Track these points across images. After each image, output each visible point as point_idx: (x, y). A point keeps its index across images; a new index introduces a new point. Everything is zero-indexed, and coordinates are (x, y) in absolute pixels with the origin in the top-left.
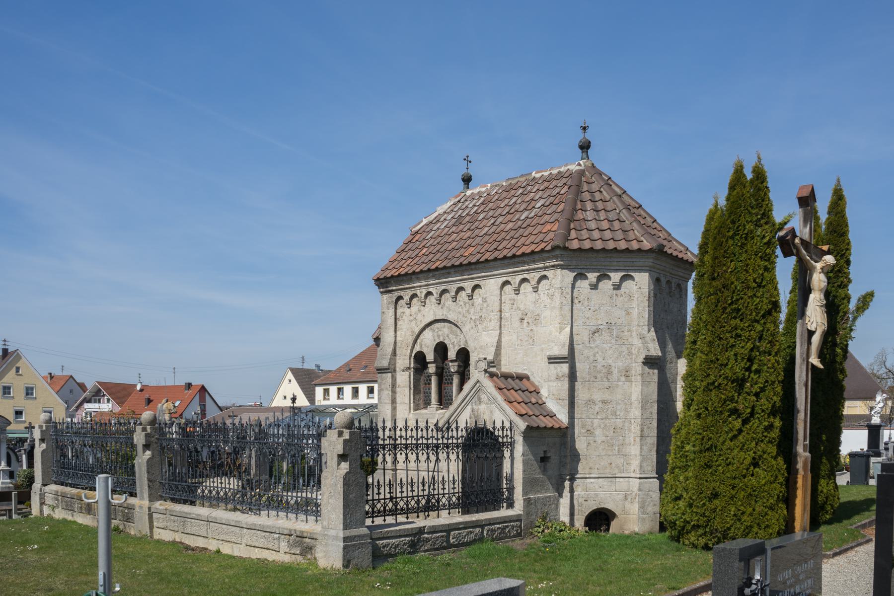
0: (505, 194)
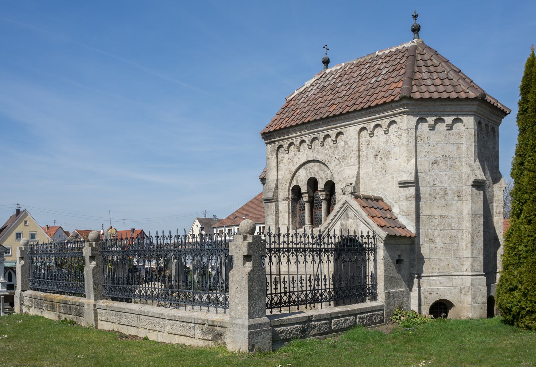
0: (356, 68)
